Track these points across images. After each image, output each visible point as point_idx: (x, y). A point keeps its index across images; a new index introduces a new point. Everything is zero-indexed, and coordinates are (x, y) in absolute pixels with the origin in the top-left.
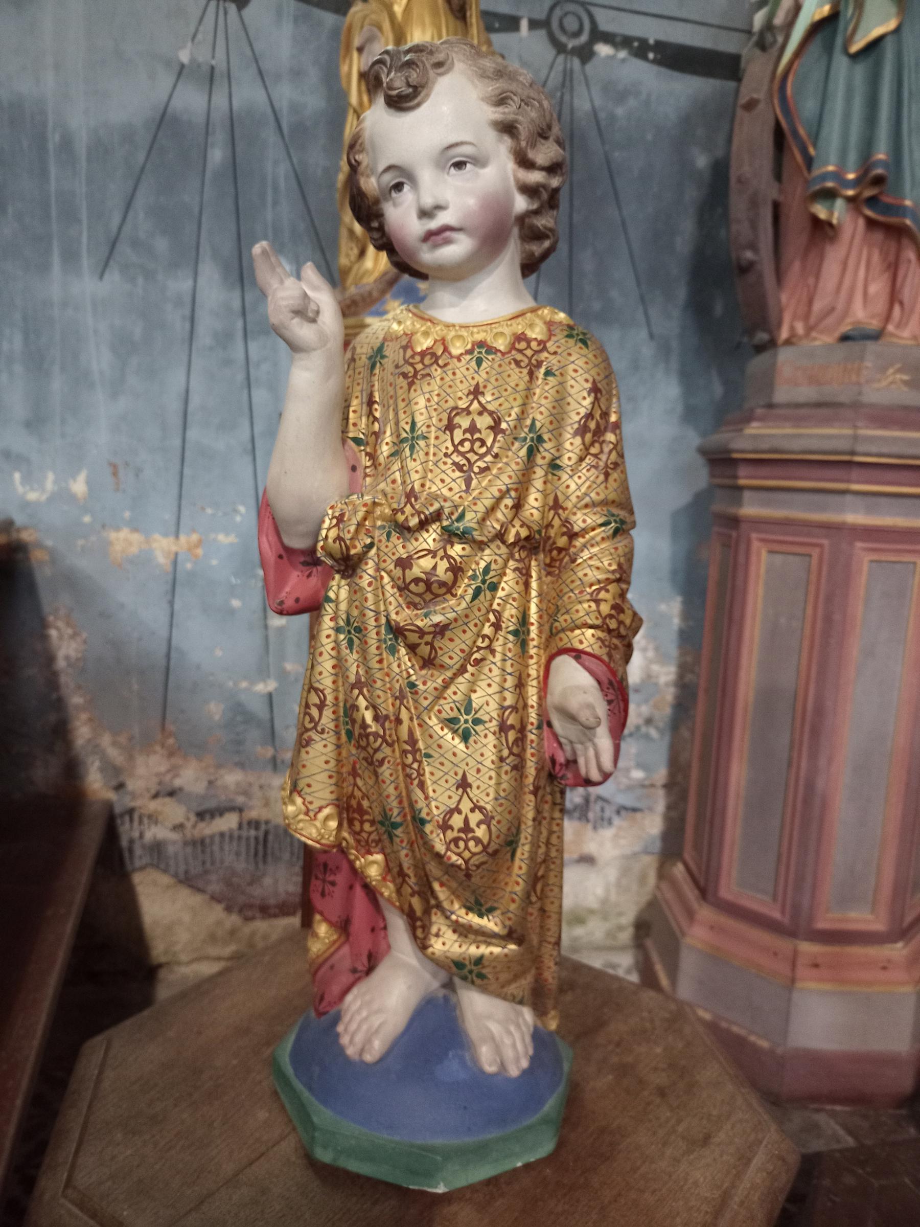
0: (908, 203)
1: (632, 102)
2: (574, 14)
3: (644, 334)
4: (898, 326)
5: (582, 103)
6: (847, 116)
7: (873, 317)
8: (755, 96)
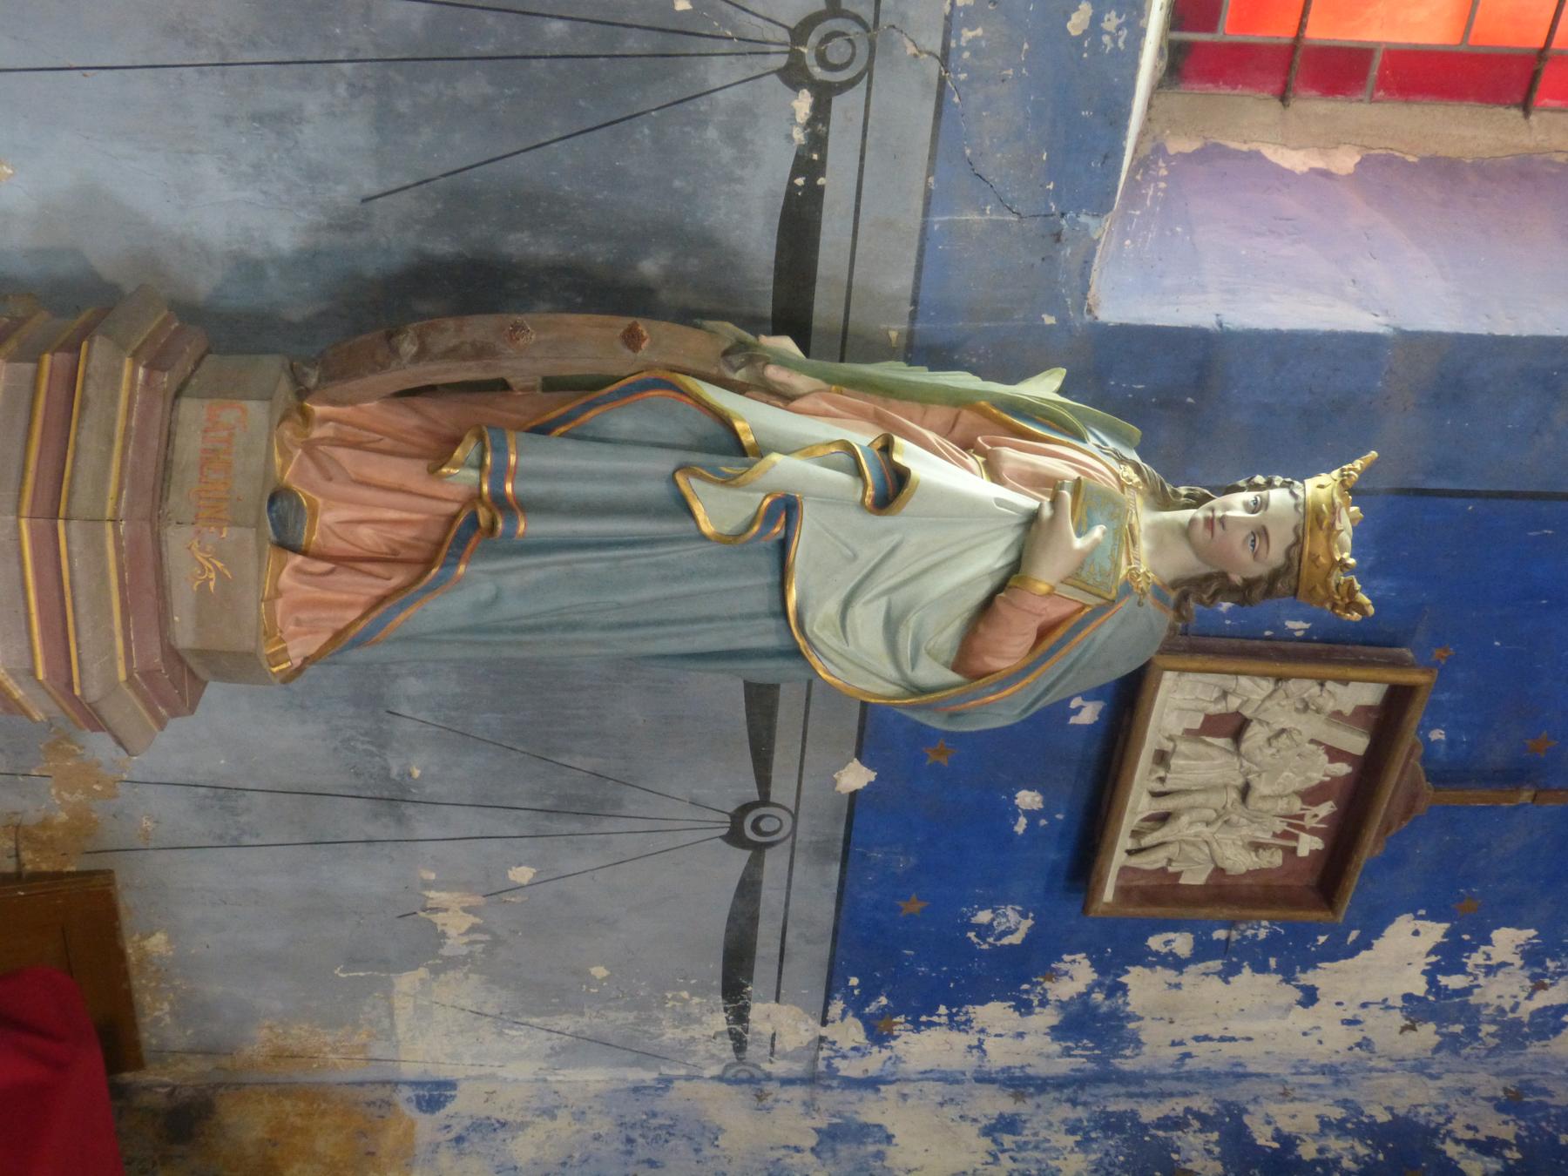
0: (462, 569)
1: (727, 153)
2: (853, 54)
3: (370, 187)
4: (298, 570)
5: (717, 72)
6: (591, 476)
7: (322, 534)
8: (644, 345)
